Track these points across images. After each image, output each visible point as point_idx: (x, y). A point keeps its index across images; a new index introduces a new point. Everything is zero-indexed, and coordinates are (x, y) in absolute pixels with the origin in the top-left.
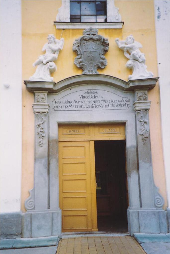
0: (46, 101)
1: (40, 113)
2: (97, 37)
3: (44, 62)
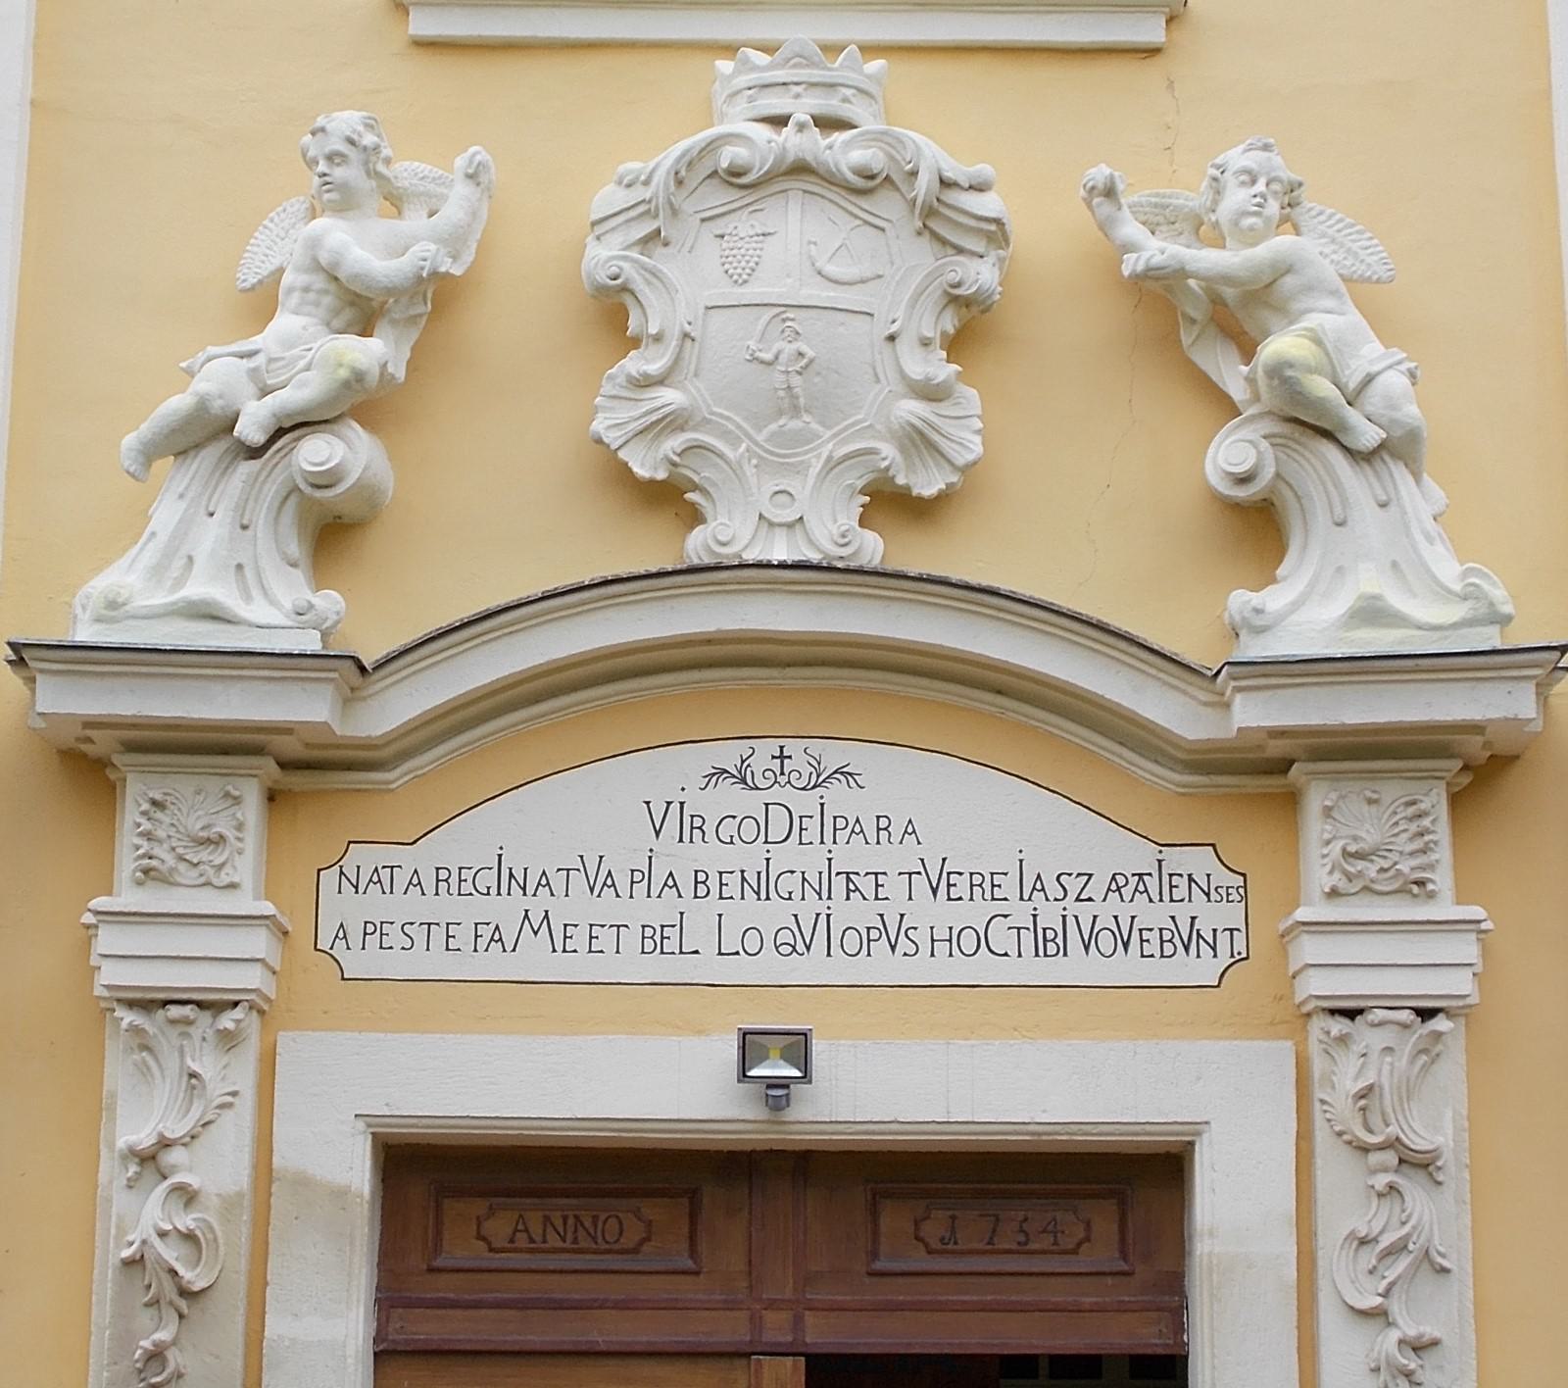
0: (245, 864)
1: (175, 1011)
2: (859, 156)
3: (251, 428)
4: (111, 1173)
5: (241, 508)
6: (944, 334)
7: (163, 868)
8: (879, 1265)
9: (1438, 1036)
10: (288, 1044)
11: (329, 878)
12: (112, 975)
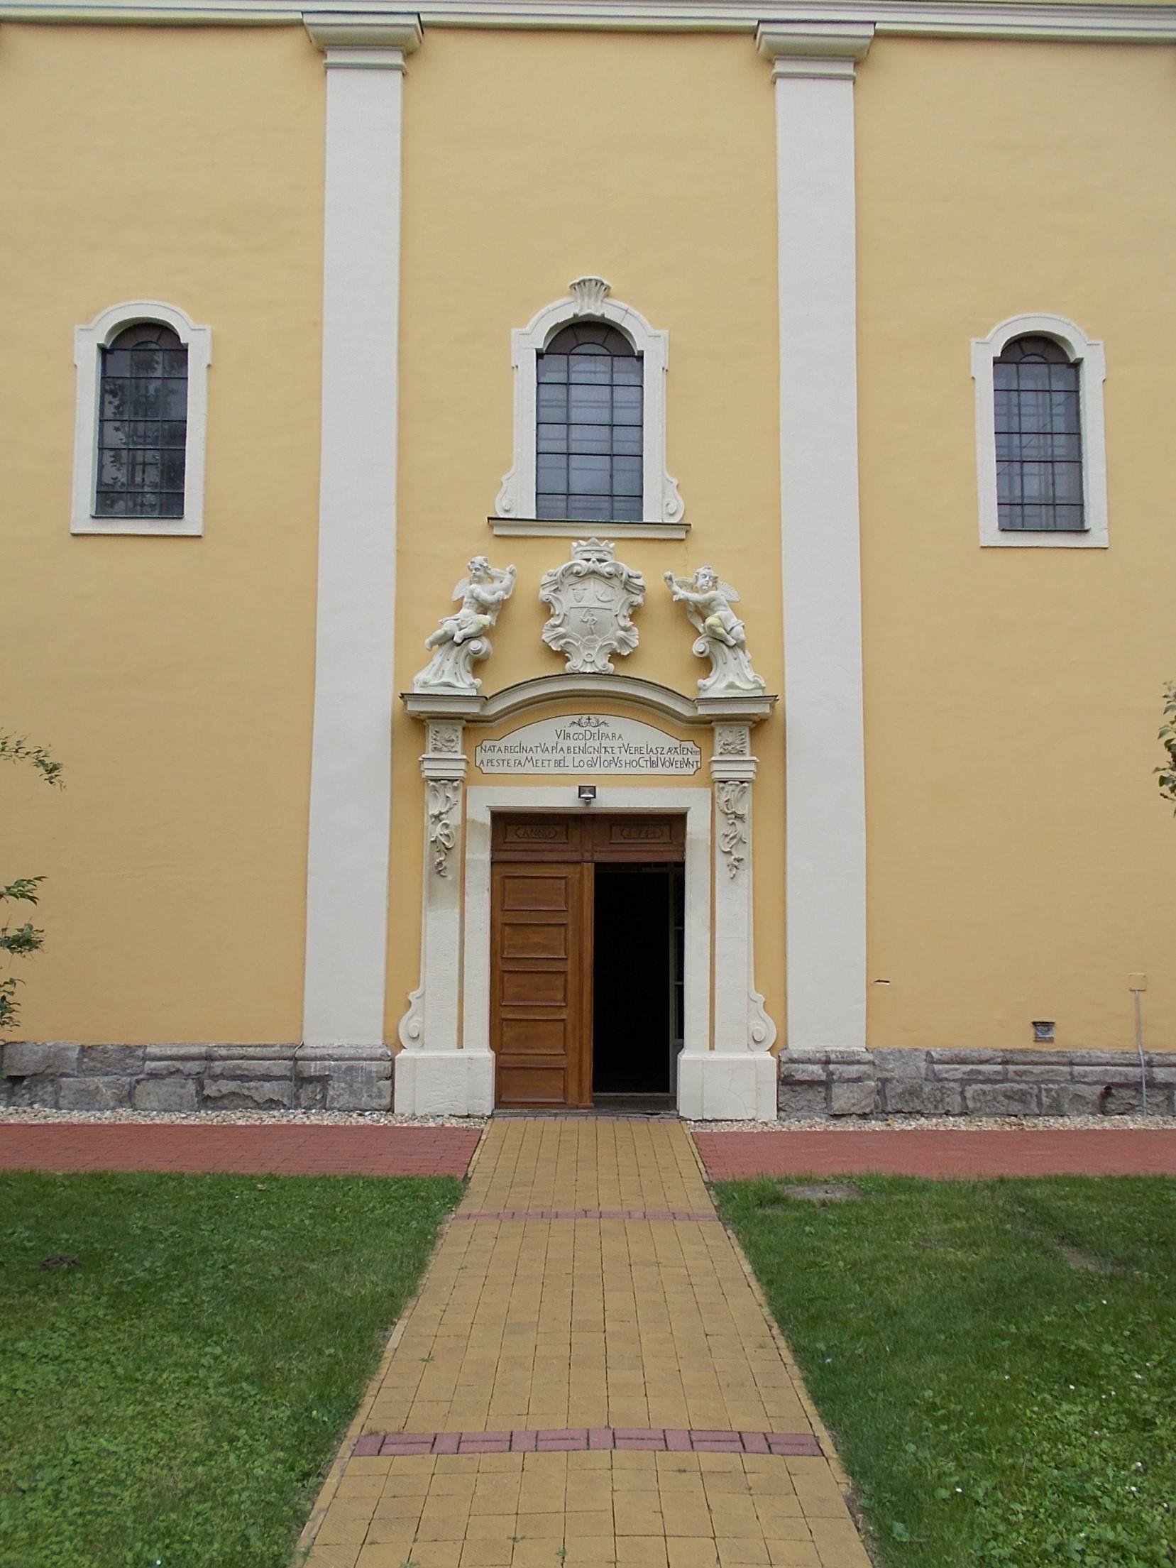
0: (459, 748)
2: (608, 569)
3: (457, 639)
4: (428, 821)
5: (456, 658)
11: (479, 748)
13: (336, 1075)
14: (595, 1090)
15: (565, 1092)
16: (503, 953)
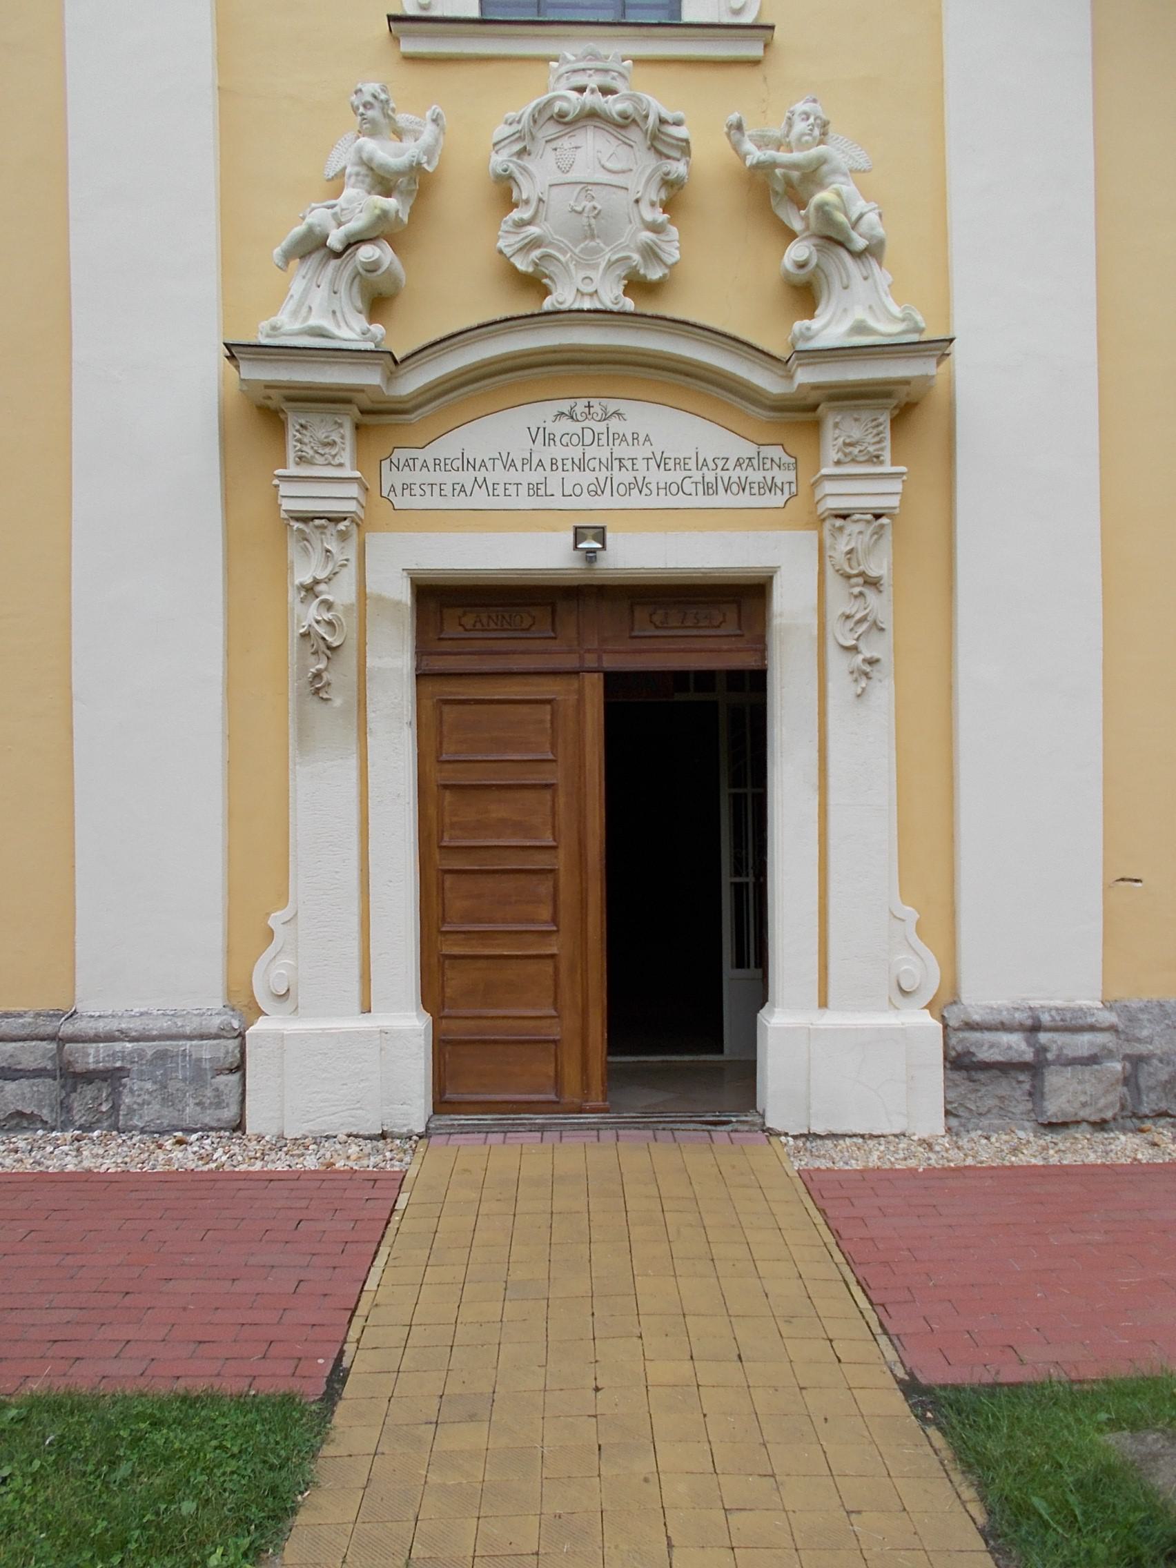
0: (346, 457)
1: (317, 522)
2: (620, 107)
3: (335, 241)
4: (293, 597)
5: (333, 282)
6: (661, 200)
7: (309, 456)
8: (635, 633)
9: (882, 526)
10: (372, 539)
11: (386, 464)
12: (287, 505)
13: (135, 1067)
14: (609, 1053)
15: (558, 1083)
16: (441, 838)
